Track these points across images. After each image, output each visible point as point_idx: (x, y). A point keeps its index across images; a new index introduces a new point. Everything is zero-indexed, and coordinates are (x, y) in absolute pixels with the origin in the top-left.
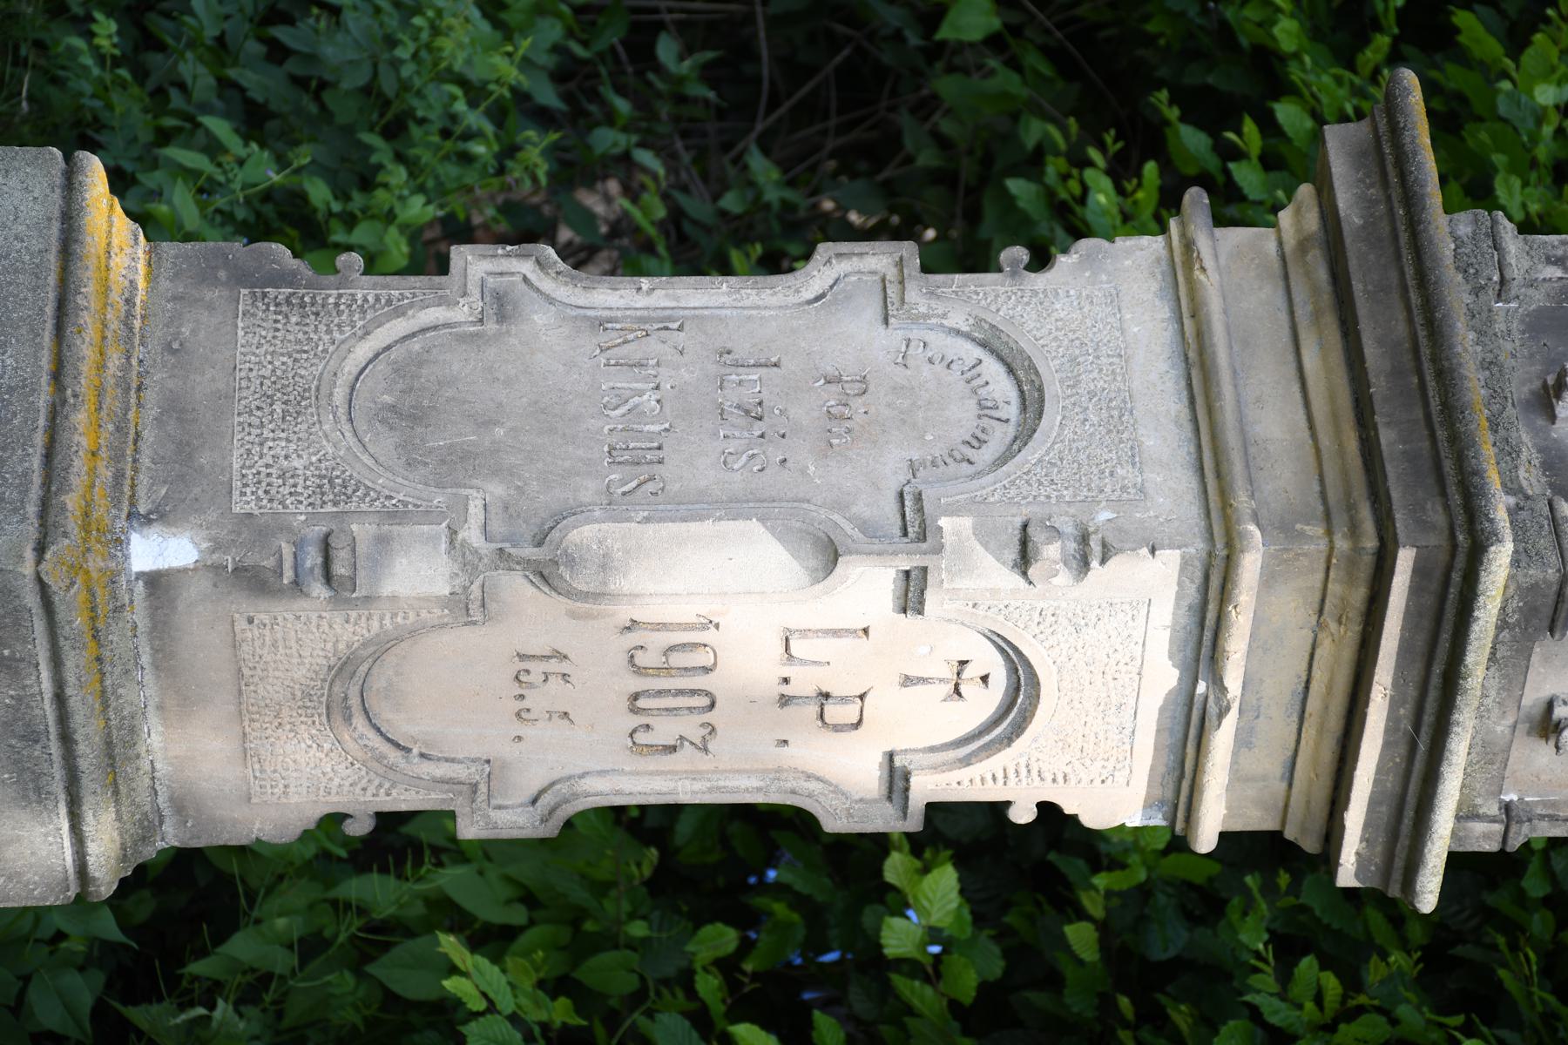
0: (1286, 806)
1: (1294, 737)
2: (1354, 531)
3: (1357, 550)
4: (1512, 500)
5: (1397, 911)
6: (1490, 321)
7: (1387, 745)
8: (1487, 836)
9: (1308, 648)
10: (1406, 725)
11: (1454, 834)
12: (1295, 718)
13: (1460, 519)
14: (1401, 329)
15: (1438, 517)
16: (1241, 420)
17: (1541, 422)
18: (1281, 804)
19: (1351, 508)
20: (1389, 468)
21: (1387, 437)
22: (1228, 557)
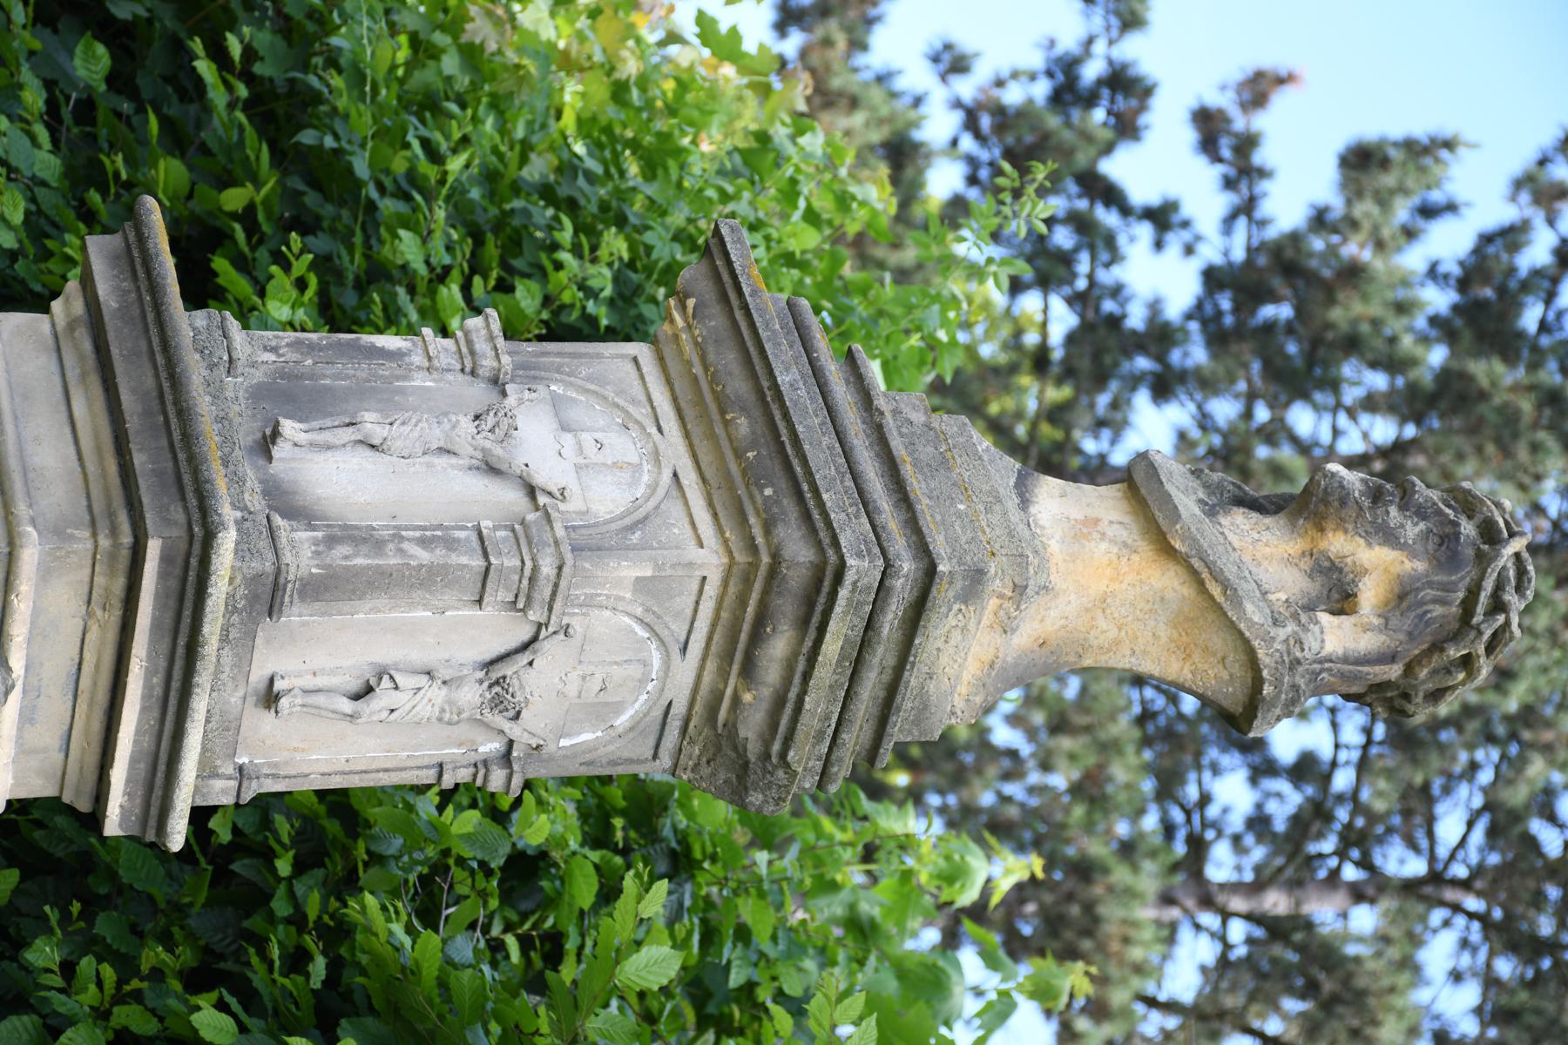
0: (64, 774)
1: (69, 713)
2: (114, 532)
3: (116, 545)
4: (239, 514)
5: (157, 849)
6: (222, 389)
7: (144, 710)
8: (224, 791)
9: (80, 634)
10: (158, 691)
11: (197, 790)
12: (70, 696)
13: (196, 516)
14: (150, 382)
15: (178, 514)
16: (21, 450)
17: (261, 462)
18: (59, 773)
19: (111, 515)
20: (141, 481)
21: (139, 459)
22: (10, 554)
